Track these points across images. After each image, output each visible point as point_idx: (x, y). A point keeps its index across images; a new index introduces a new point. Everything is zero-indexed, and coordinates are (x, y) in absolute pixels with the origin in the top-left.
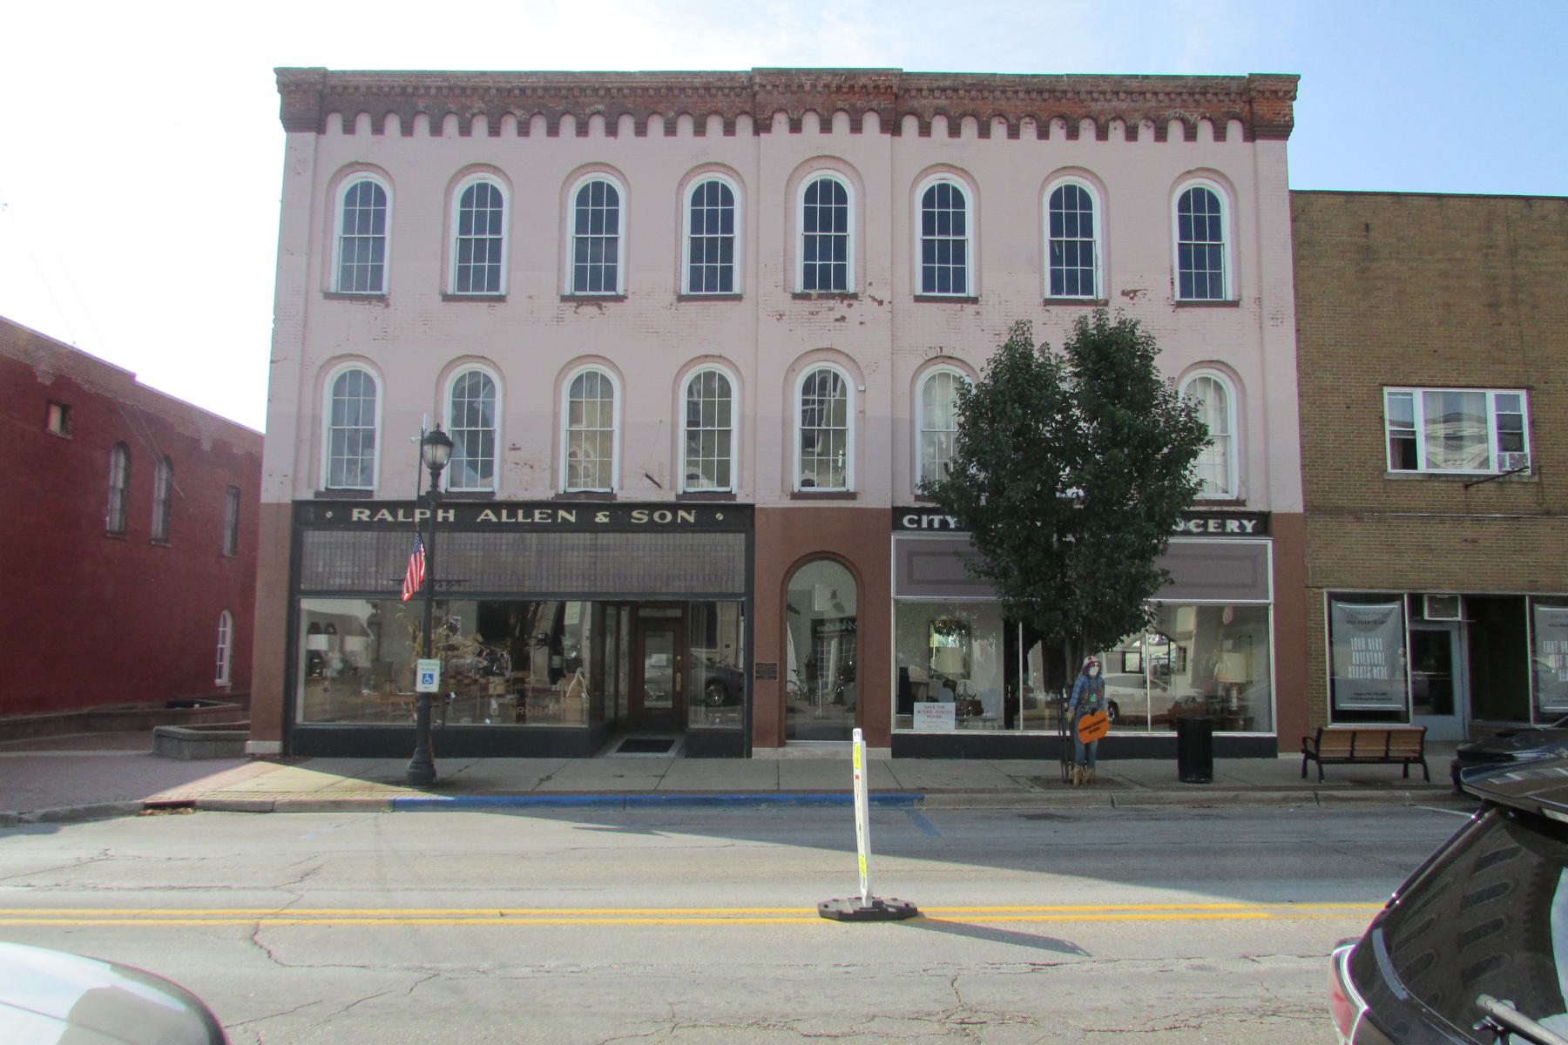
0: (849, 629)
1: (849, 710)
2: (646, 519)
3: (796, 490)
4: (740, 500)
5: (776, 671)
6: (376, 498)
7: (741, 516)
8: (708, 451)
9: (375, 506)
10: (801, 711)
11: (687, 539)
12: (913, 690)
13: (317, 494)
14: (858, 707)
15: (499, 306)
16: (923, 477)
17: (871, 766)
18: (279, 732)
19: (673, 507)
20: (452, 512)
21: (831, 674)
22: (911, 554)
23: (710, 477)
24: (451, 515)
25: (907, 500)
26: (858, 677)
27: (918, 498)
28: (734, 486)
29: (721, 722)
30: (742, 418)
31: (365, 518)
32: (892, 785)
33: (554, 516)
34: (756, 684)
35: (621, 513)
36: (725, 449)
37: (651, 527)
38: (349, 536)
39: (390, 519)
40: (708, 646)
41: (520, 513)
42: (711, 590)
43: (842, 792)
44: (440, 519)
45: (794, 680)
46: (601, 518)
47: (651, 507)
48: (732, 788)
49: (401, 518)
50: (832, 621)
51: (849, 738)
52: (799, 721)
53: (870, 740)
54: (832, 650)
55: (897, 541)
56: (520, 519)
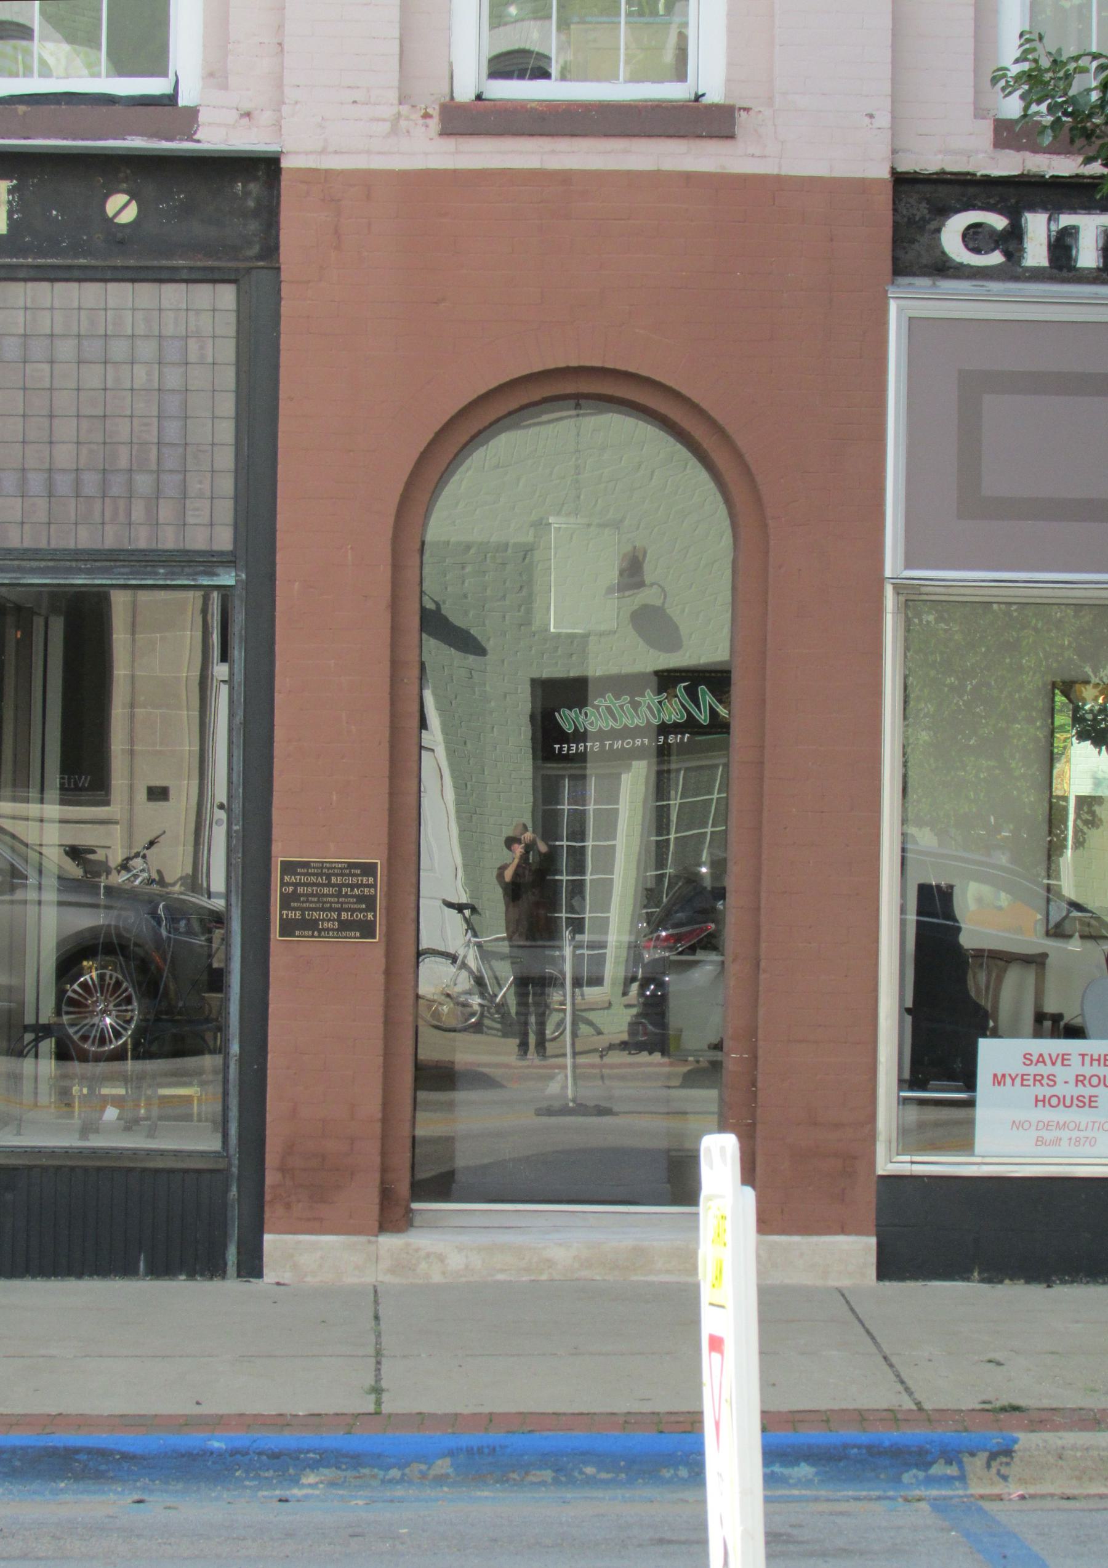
0: (699, 710)
1: (691, 1079)
3: (465, 93)
4: (215, 136)
5: (371, 902)
7: (215, 205)
10: (481, 1080)
12: (977, 981)
14: (733, 1059)
16: (1030, 40)
17: (779, 1312)
21: (614, 911)
22: (973, 386)
23: (78, 35)
25: (962, 145)
26: (733, 932)
27: (1007, 135)
29: (130, 1125)
32: (878, 1394)
34: (282, 952)
40: (71, 794)
42: (84, 539)
43: (659, 1422)
45: (454, 945)
48: (177, 1405)
50: (622, 684)
51: (679, 1182)
52: (471, 1124)
53: (780, 1212)
54: (621, 815)
55: (914, 325)
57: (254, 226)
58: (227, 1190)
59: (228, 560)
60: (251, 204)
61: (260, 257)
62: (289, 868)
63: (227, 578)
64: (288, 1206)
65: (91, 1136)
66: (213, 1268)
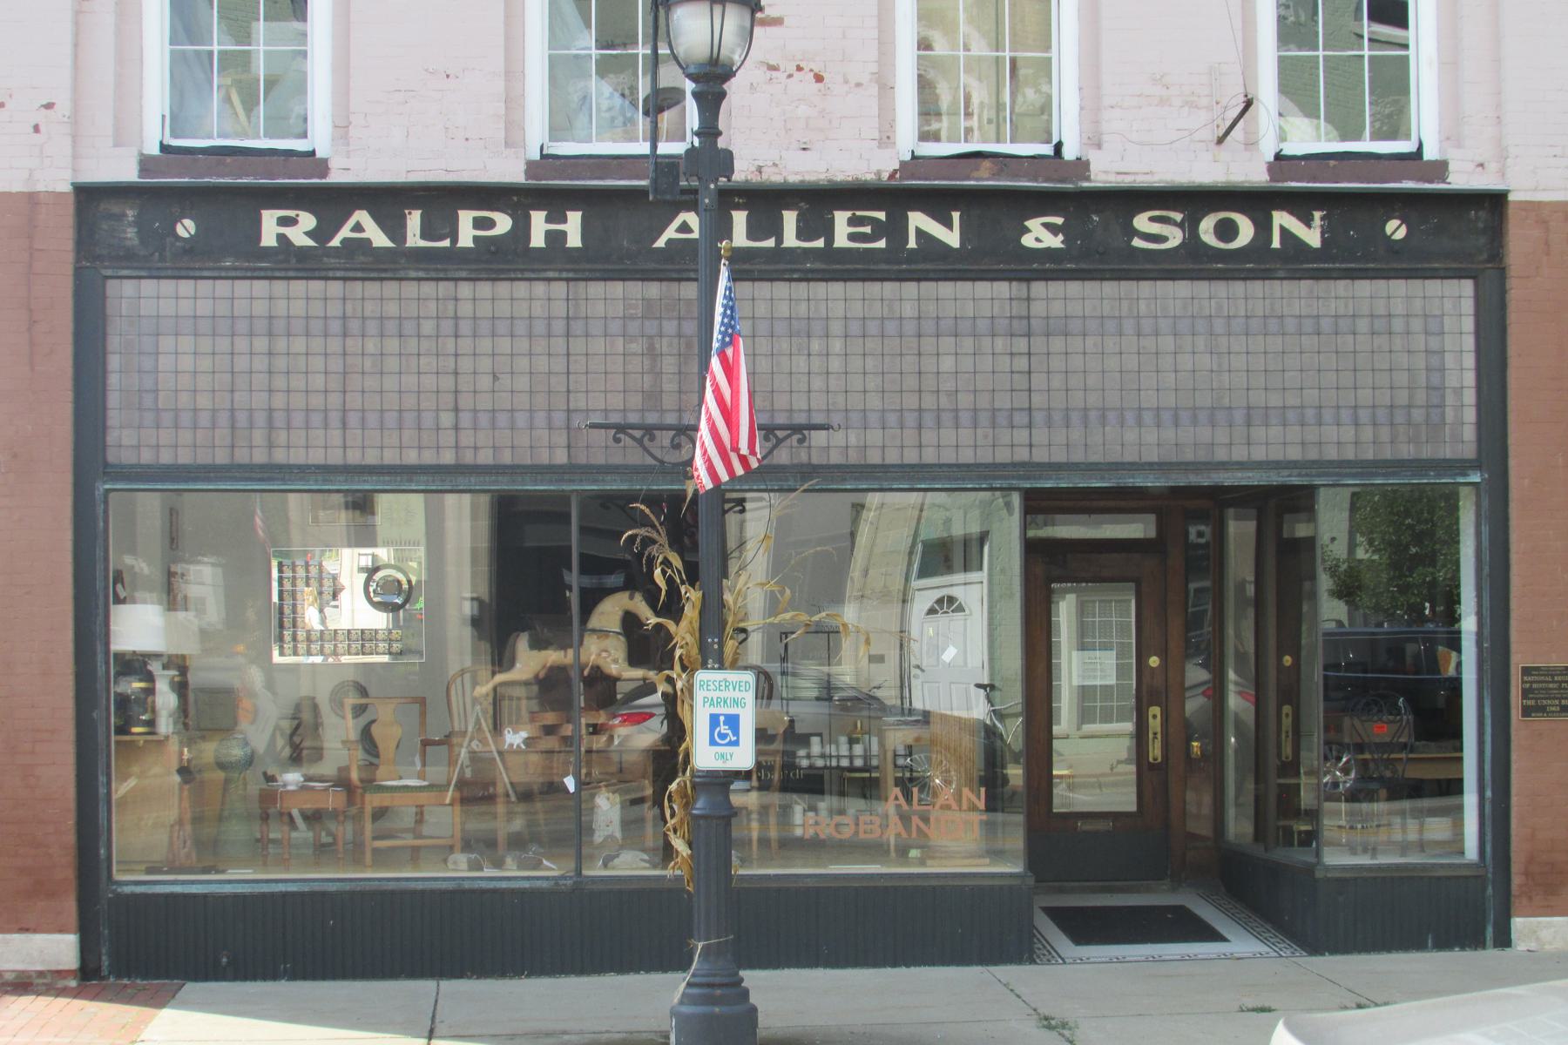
2: (1175, 238)
4: (1461, 178)
6: (336, 177)
9: (334, 201)
11: (1293, 297)
13: (146, 164)
18: (70, 906)
19: (1257, 202)
20: (574, 219)
24: (573, 227)
28: (1427, 128)
31: (299, 236)
33: (895, 228)
35: (1101, 223)
37: (1193, 263)
38: (252, 296)
39: (380, 239)
41: (790, 219)
44: (538, 240)
46: (1039, 234)
47: (1192, 201)
49: (414, 237)
56: (790, 240)
57: (1482, 240)
58: (1484, 889)
59: (1476, 465)
60: (1481, 225)
61: (1488, 261)
62: (1526, 671)
63: (1475, 478)
64: (1530, 898)
65: (929, 862)
66: (1477, 942)
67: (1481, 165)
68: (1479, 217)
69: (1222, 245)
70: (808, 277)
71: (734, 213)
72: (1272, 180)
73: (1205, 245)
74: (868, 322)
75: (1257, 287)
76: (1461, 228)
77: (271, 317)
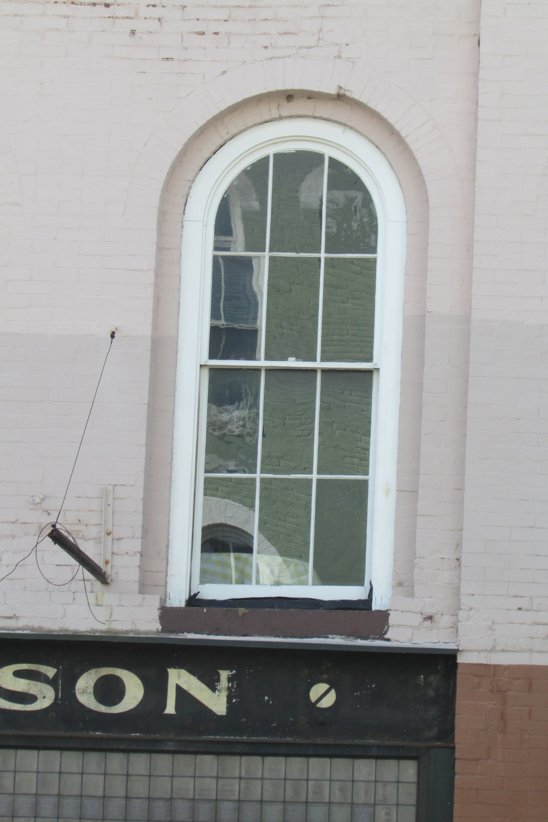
2: (45, 697)
4: (404, 634)
8: (288, 453)
11: (199, 775)
13: (167, 615)
15: (98, 584)
19: (149, 656)
23: (288, 546)
30: (416, 327)
36: (351, 442)
61: (438, 738)
67: (430, 618)
68: (428, 681)
69: (102, 709)
70: (129, 748)
71: (221, 672)
72: (164, 630)
73: (82, 707)
74: (335, 808)
75: (140, 762)
76: (404, 697)
77: (149, 799)
